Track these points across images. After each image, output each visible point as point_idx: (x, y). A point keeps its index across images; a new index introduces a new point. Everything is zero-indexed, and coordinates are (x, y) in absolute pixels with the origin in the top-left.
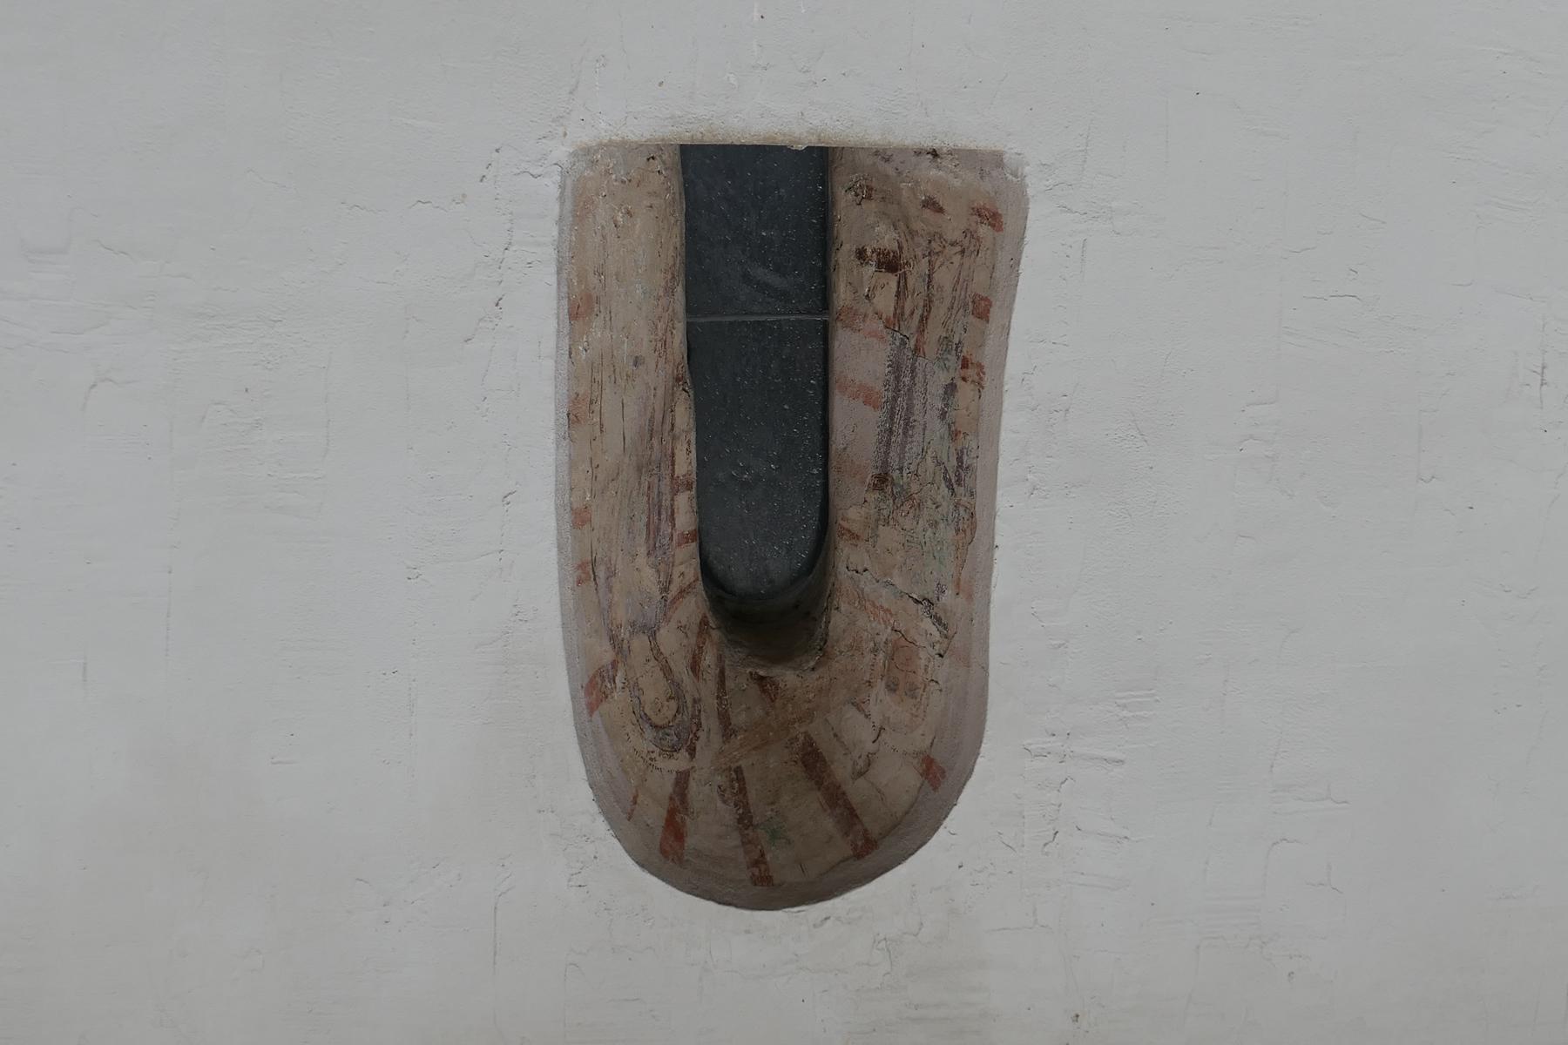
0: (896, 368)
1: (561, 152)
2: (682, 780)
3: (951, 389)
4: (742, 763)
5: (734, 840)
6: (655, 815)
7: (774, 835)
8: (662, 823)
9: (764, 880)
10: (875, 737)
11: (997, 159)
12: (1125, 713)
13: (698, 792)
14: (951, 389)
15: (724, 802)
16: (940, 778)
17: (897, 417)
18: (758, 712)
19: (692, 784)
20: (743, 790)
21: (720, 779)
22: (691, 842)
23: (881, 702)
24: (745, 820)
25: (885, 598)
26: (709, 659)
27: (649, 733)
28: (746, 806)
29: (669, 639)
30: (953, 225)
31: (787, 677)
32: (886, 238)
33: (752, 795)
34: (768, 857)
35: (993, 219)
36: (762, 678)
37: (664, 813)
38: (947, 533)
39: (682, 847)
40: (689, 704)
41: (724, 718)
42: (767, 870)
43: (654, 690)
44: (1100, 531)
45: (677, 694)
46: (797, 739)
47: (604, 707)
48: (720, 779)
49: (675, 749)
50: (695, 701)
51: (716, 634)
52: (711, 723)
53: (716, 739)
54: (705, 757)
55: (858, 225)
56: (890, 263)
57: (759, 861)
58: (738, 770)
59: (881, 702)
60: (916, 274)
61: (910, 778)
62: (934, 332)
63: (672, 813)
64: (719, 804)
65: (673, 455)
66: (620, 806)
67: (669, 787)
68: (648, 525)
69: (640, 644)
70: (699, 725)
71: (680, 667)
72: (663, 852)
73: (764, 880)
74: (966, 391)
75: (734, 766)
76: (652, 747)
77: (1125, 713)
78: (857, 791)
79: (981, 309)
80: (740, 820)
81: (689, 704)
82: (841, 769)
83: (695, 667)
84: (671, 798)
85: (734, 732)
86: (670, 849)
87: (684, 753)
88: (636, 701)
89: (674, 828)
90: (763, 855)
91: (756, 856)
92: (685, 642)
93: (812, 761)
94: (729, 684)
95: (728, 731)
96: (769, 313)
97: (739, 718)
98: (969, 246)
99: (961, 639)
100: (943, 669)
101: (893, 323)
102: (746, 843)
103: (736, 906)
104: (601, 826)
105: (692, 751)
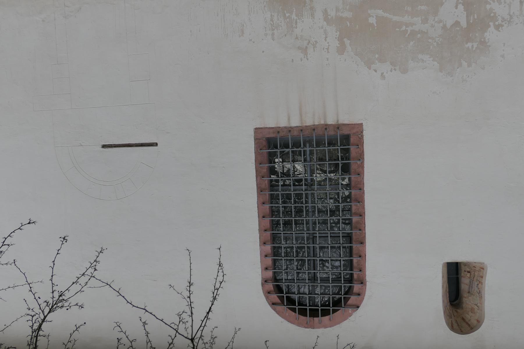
0: (470, 282)
1: (442, 263)
3: (478, 284)
6: (450, 325)
9: (462, 331)
10: (472, 318)
11: (484, 263)
14: (478, 284)
16: (479, 322)
17: (471, 285)
23: (470, 314)
24: (458, 325)
25: (470, 304)
30: (477, 269)
31: (459, 311)
32: (468, 270)
35: (483, 269)
38: (478, 298)
44: (495, 298)
55: (463, 268)
56: (469, 272)
59: (470, 314)
60: (472, 273)
61: (476, 322)
62: (475, 279)
66: (448, 324)
73: (462, 331)
74: (480, 285)
78: (469, 323)
79: (482, 277)
82: (467, 320)
86: (452, 328)
93: (463, 319)
96: (336, 244)
98: (479, 271)
99: (480, 307)
100: (478, 311)
101: (470, 278)
104: (447, 326)
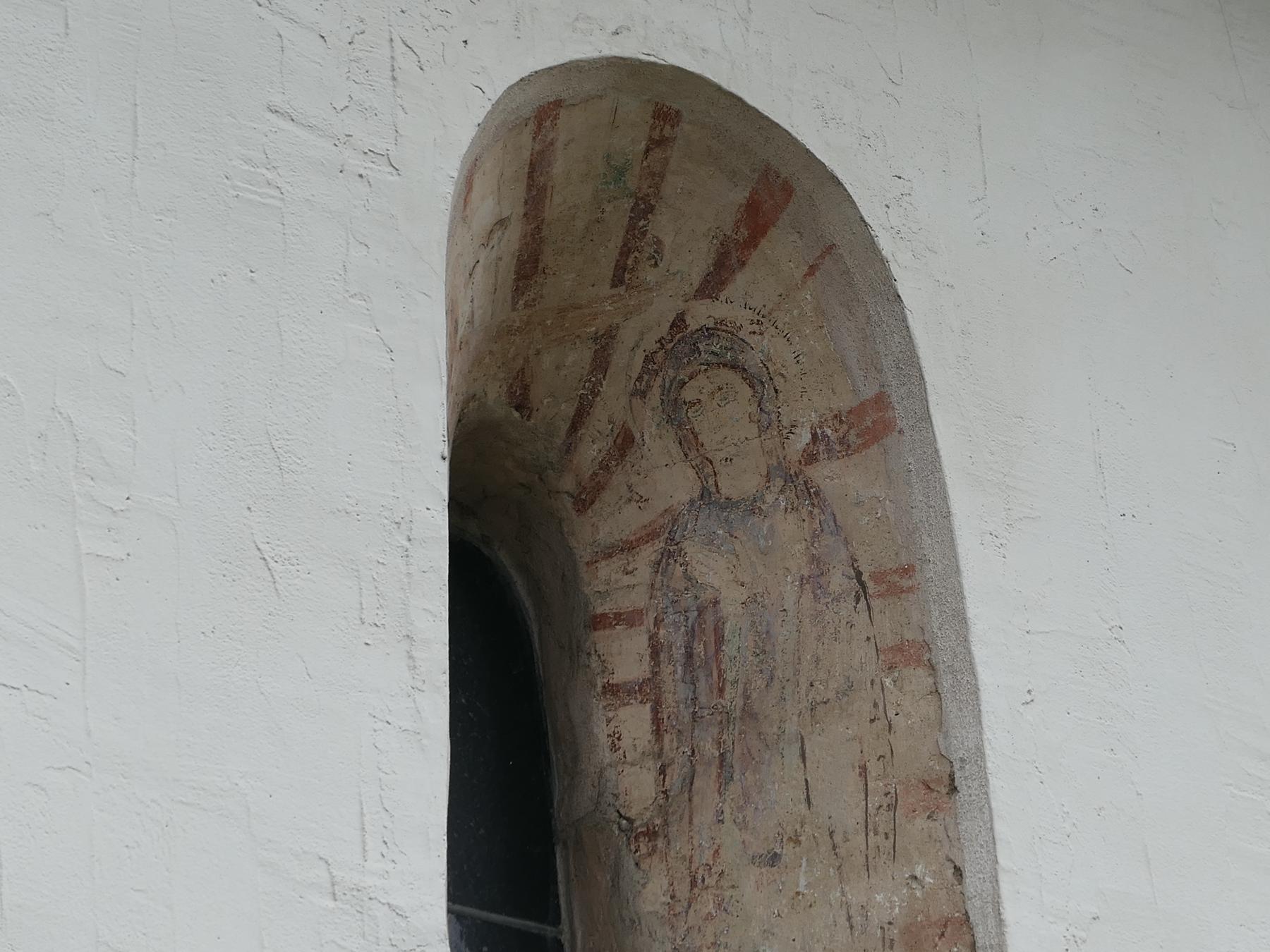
2: (712, 286)
4: (606, 290)
5: (673, 184)
7: (621, 172)
8: (773, 233)
12: (269, 175)
13: (693, 263)
15: (659, 242)
18: (547, 361)
19: (696, 280)
20: (625, 251)
21: (650, 275)
22: (740, 196)
24: (644, 208)
26: (591, 452)
27: (752, 360)
28: (631, 227)
29: (673, 484)
33: (615, 243)
34: (643, 146)
36: (518, 408)
37: (764, 243)
39: (754, 192)
40: (656, 391)
41: (601, 364)
42: (653, 128)
43: (726, 420)
45: (676, 412)
46: (526, 305)
47: (844, 402)
48: (650, 275)
49: (709, 332)
50: (643, 394)
51: (568, 483)
52: (627, 359)
53: (627, 335)
54: (662, 309)
57: (658, 142)
58: (617, 281)
63: (752, 242)
64: (667, 240)
65: (658, 732)
66: (847, 266)
67: (741, 280)
68: (720, 640)
69: (740, 481)
70: (649, 359)
71: (657, 444)
72: (788, 190)
75: (622, 290)
76: (752, 340)
77: (269, 175)
80: (651, 209)
81: (656, 391)
83: (625, 443)
84: (743, 264)
85: (595, 339)
87: (693, 324)
88: (768, 406)
89: (756, 220)
90: (647, 151)
91: (657, 154)
92: (635, 479)
94: (568, 410)
95: (604, 343)
97: (579, 357)
102: (657, 177)
103: (719, 88)
105: (679, 323)
